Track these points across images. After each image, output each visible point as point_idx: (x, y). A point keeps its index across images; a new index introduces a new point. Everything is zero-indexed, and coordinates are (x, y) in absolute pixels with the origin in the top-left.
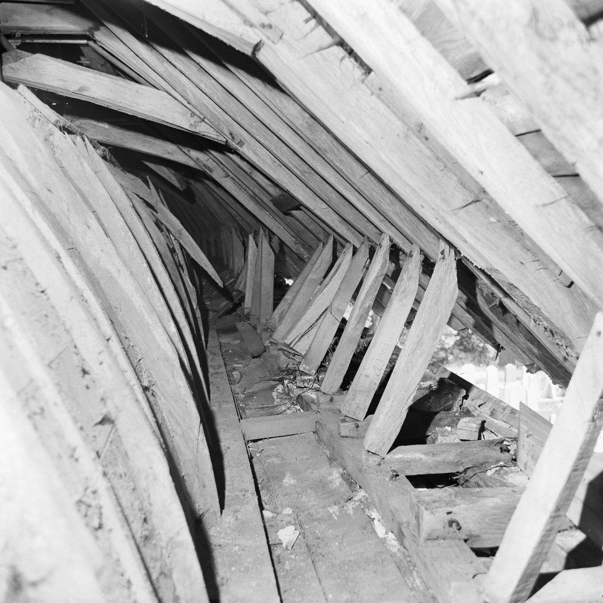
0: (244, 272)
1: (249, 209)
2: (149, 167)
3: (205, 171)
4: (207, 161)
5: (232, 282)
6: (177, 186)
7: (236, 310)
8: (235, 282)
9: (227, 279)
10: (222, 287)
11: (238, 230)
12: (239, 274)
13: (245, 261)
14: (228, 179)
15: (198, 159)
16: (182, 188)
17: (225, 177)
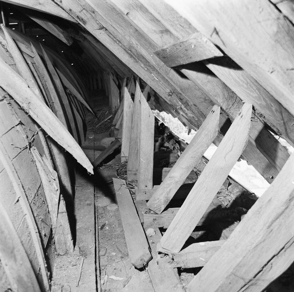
0: (120, 111)
1: (124, 62)
2: (33, 20)
3: (79, 23)
4: (80, 12)
5: (111, 118)
6: (64, 42)
7: (115, 157)
8: (113, 118)
9: (107, 114)
10: (92, 173)
11: (114, 75)
12: (116, 112)
13: (120, 101)
14: (102, 31)
15: (70, 10)
16: (69, 43)
17: (100, 29)
